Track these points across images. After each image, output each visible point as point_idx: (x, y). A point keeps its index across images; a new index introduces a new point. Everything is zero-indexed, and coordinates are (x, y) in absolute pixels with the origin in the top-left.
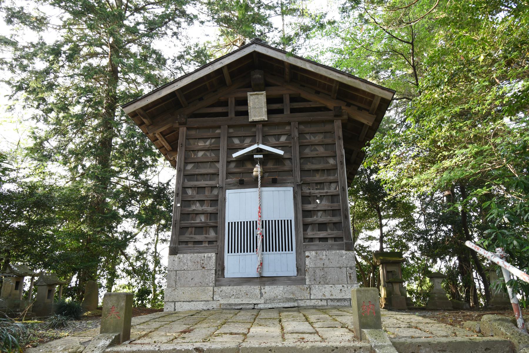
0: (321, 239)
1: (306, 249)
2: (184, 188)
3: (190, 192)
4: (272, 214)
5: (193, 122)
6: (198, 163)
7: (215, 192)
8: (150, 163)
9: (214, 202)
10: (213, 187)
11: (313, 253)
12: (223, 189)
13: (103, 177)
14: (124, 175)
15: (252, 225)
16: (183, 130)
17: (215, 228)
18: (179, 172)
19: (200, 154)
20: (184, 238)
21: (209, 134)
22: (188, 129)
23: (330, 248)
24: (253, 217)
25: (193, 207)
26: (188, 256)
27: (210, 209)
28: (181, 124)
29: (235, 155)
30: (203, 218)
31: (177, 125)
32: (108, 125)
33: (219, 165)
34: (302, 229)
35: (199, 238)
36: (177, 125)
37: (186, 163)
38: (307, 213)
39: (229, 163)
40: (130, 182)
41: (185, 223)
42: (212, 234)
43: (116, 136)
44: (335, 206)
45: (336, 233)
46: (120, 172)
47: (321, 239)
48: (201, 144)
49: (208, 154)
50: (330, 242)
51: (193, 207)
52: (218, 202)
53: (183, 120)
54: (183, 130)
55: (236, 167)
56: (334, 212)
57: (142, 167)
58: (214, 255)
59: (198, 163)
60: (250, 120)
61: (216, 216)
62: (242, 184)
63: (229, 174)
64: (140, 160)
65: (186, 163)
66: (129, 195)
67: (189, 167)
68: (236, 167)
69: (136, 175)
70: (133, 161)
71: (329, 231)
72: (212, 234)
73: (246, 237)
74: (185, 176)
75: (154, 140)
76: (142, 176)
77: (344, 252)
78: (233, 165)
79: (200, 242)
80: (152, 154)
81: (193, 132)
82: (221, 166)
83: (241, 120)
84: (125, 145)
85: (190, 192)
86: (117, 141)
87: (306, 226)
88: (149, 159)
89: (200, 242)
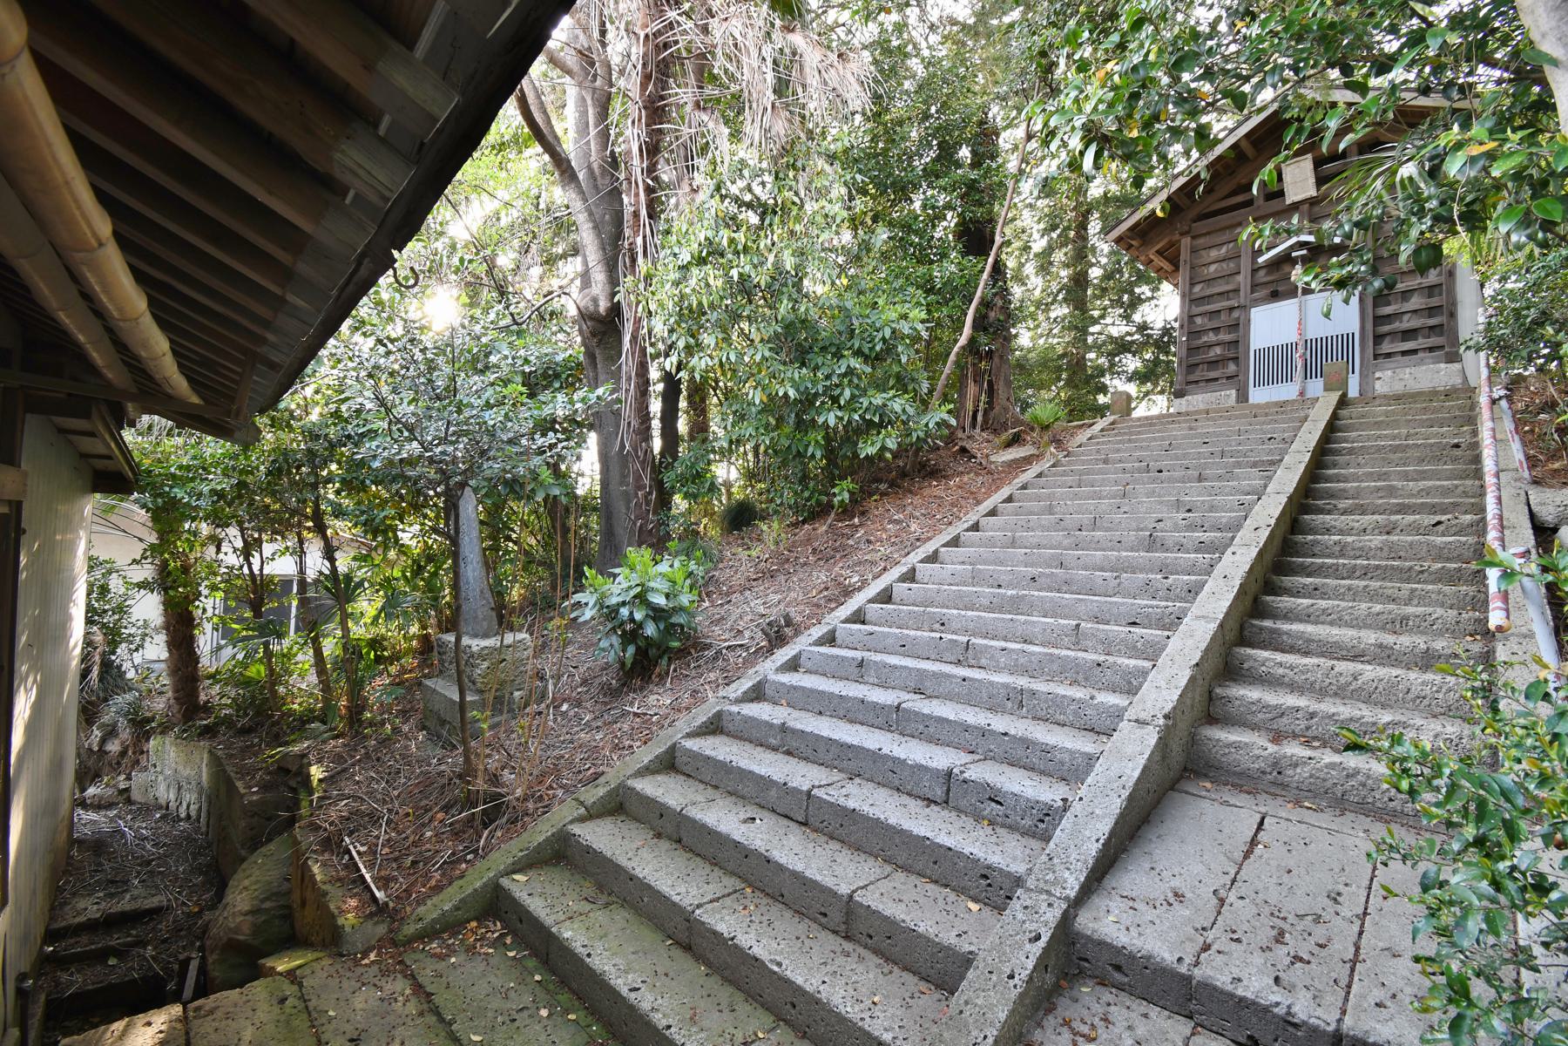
0: (1404, 353)
1: (1377, 368)
2: (1191, 317)
3: (1199, 320)
4: (1319, 329)
5: (1200, 227)
6: (1210, 281)
7: (1236, 314)
8: (1149, 294)
9: (1235, 326)
10: (1231, 309)
11: (1389, 373)
12: (1245, 308)
13: (1080, 325)
14: (1108, 320)
15: (1292, 347)
16: (1186, 242)
17: (1235, 359)
18: (1183, 296)
19: (1213, 268)
20: (1192, 378)
21: (1224, 238)
22: (1193, 238)
23: (1422, 362)
24: (1293, 337)
25: (1205, 339)
26: (1199, 397)
27: (1225, 337)
28: (1182, 234)
29: (1261, 260)
30: (1218, 350)
31: (1177, 237)
32: (1081, 254)
33: (1240, 278)
34: (1371, 344)
35: (1213, 375)
36: (1177, 237)
37: (1192, 285)
38: (1379, 320)
39: (1255, 271)
40: (1118, 329)
41: (1194, 360)
42: (1232, 367)
43: (1093, 265)
44: (1434, 302)
45: (1434, 341)
46: (1103, 317)
47: (1404, 353)
48: (1214, 253)
49: (1224, 265)
50: (1421, 355)
51: (1205, 339)
52: (1239, 328)
53: (1186, 228)
54: (1186, 242)
55: (1267, 274)
56: (1431, 311)
57: (1136, 302)
58: (1234, 392)
59: (1210, 281)
60: (1288, 202)
61: (1236, 348)
62: (1275, 296)
63: (1255, 287)
64: (1132, 293)
65: (1192, 285)
66: (1122, 346)
67: (1197, 289)
68: (1267, 274)
69: (1127, 318)
70: (1121, 298)
71: (1421, 340)
72: (1232, 367)
73: (1279, 364)
74: (1191, 301)
75: (1149, 262)
76: (1137, 317)
77: (1443, 366)
78: (1262, 272)
79: (1216, 379)
80: (1148, 281)
81: (1201, 241)
82: (1243, 280)
83: (1274, 205)
84: (1108, 276)
85: (1199, 320)
86: (1095, 273)
87: (1378, 339)
88: (1144, 290)
89: (1216, 379)
